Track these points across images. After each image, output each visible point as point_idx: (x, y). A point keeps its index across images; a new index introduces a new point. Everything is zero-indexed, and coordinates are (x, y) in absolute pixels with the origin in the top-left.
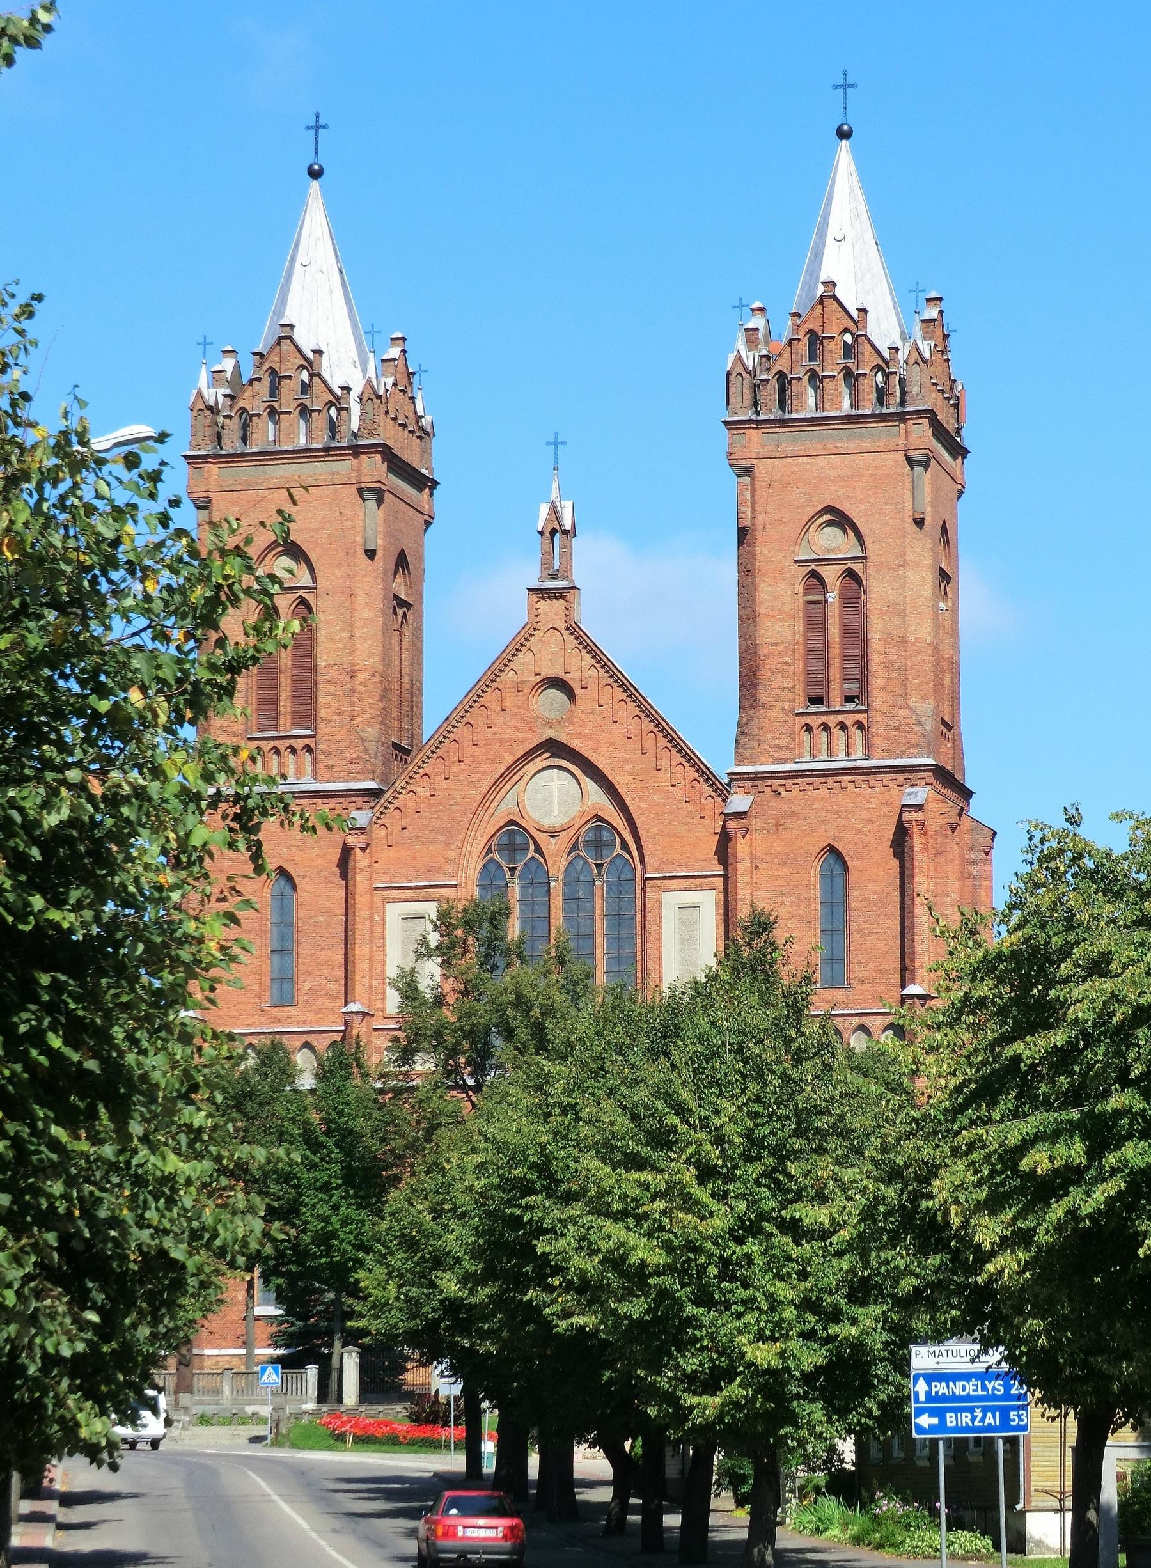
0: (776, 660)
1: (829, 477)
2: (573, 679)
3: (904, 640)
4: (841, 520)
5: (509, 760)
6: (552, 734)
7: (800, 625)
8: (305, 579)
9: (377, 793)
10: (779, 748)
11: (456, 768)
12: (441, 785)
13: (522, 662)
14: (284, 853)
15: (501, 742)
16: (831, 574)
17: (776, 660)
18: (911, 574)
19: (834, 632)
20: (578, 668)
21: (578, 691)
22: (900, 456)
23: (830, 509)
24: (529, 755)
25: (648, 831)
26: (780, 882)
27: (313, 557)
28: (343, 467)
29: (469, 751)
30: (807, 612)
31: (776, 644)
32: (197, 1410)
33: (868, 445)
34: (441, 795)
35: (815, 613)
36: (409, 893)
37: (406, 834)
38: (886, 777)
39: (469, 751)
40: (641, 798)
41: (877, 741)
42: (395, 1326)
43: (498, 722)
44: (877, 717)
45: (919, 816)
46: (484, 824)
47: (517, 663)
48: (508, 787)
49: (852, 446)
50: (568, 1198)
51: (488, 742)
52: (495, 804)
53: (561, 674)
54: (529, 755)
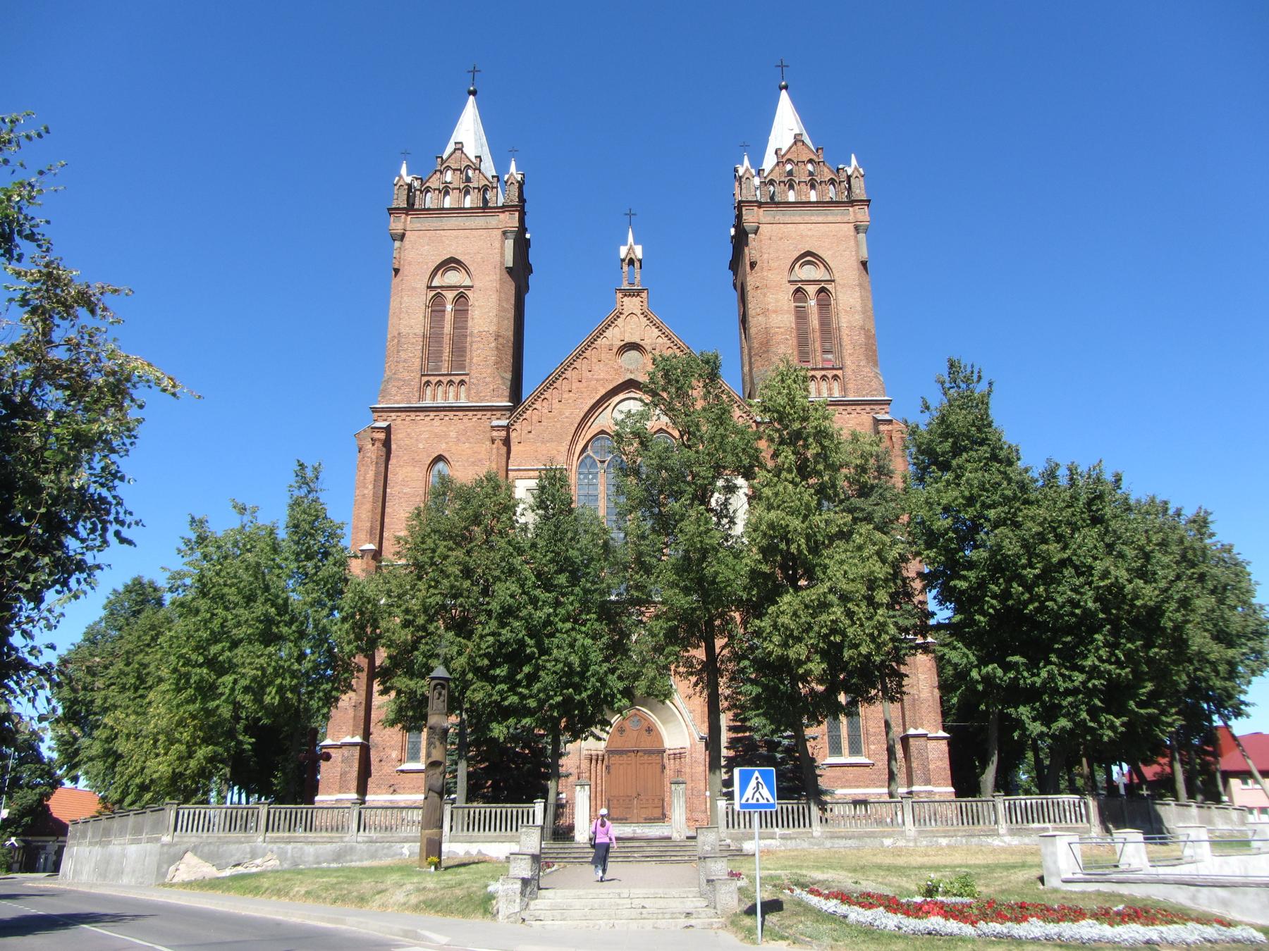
0: (780, 337)
5: (603, 392)
6: (632, 377)
7: (793, 319)
11: (566, 396)
12: (556, 405)
14: (444, 446)
16: (811, 290)
17: (780, 337)
22: (851, 226)
23: (809, 253)
27: (472, 268)
29: (575, 385)
30: (797, 312)
32: (244, 628)
33: (831, 219)
34: (555, 412)
35: (801, 315)
38: (858, 408)
41: (851, 386)
42: (770, 653)
43: (595, 368)
44: (848, 371)
45: (890, 427)
47: (608, 333)
49: (820, 219)
50: (308, 893)
51: (589, 380)
53: (638, 341)
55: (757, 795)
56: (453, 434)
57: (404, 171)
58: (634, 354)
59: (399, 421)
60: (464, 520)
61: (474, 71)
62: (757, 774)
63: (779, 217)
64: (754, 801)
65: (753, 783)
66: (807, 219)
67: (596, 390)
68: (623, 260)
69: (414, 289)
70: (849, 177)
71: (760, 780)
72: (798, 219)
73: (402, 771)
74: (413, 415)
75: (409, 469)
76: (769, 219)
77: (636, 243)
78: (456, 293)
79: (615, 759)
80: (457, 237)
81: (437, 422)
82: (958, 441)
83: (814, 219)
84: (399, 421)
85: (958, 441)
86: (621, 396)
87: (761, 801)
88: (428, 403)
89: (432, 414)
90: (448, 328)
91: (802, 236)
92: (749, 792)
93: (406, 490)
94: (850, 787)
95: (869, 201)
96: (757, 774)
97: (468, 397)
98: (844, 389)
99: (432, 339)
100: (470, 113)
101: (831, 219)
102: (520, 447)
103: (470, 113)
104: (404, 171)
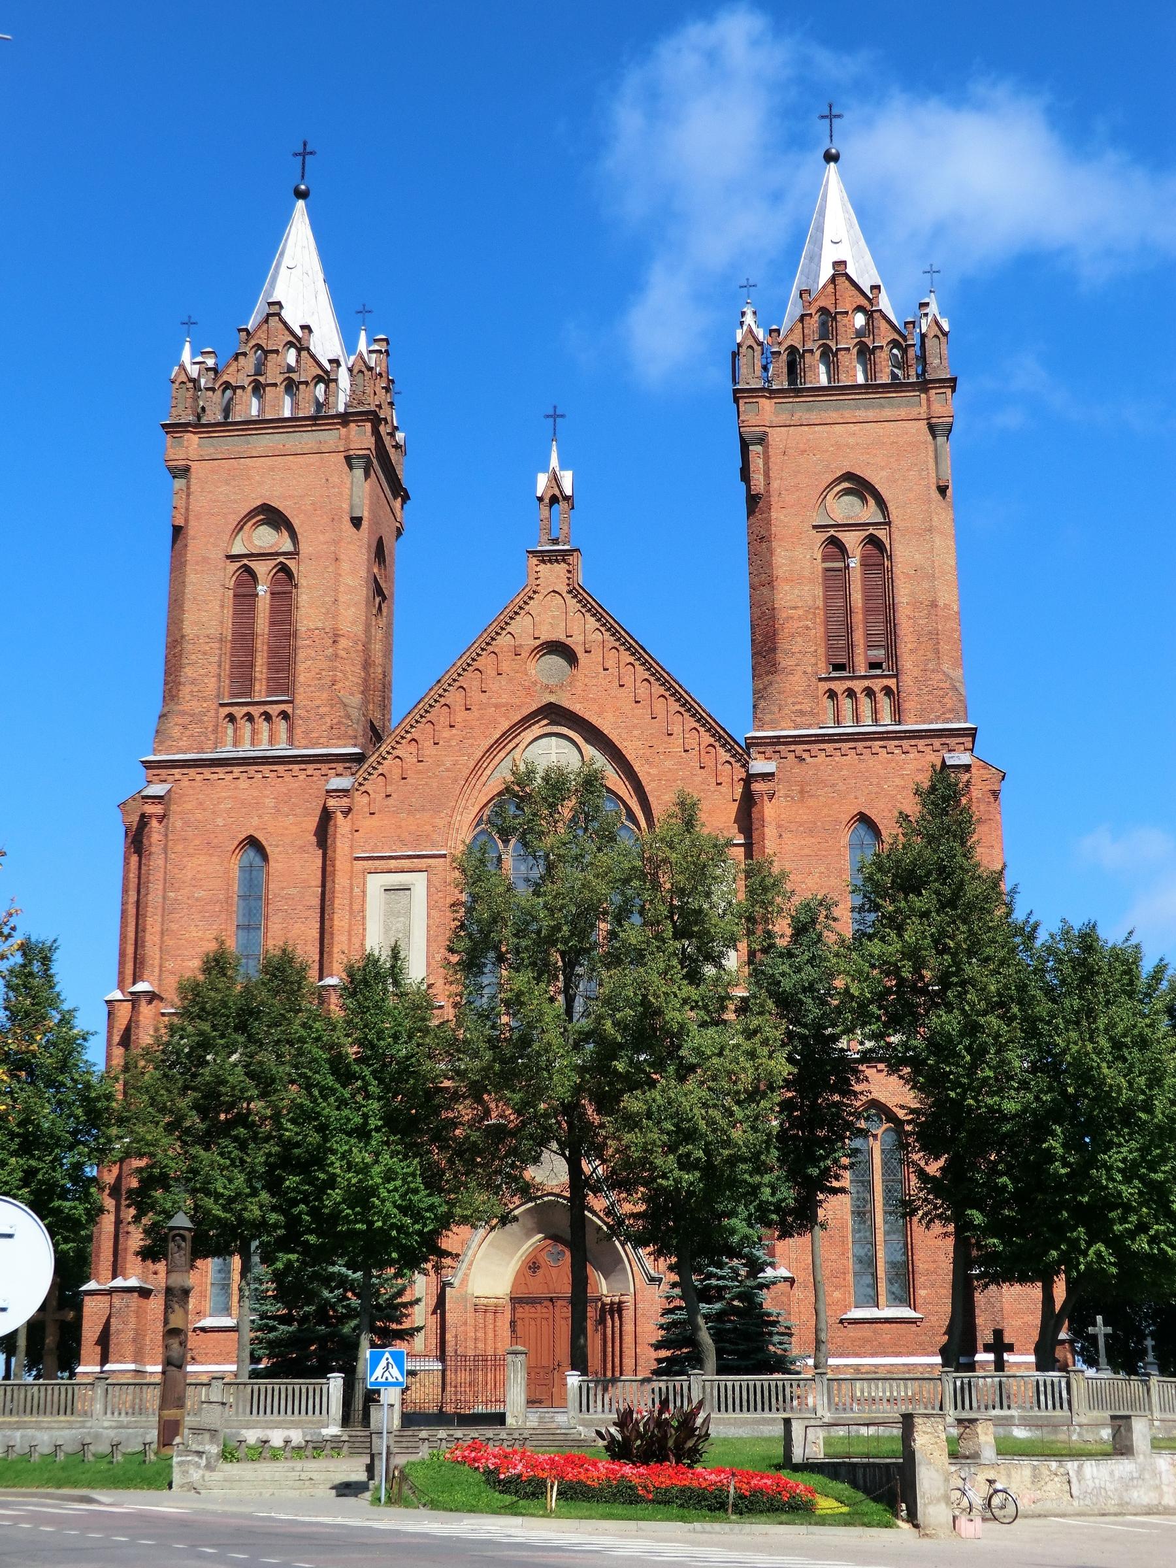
1: (847, 445)
2: (576, 643)
3: (934, 604)
4: (859, 486)
5: (506, 725)
7: (819, 591)
8: (288, 546)
9: (359, 759)
10: (802, 713)
11: (446, 733)
13: (521, 625)
14: (255, 821)
15: (496, 706)
18: (938, 541)
19: (262, 624)
20: (582, 631)
21: (580, 654)
22: (923, 425)
23: (849, 476)
24: (527, 721)
25: (658, 798)
26: (806, 851)
27: (296, 523)
28: (331, 438)
29: (460, 716)
31: (795, 608)
35: (835, 580)
36: (393, 864)
37: (390, 801)
39: (460, 716)
40: (651, 764)
43: (493, 685)
46: (475, 793)
47: (513, 627)
48: (502, 754)
52: (488, 772)
54: (527, 721)
55: (387, 1374)
56: (269, 802)
57: (186, 356)
58: (556, 661)
59: (185, 783)
60: (239, 1007)
61: (304, 154)
62: (387, 1355)
63: (801, 415)
64: (384, 1380)
65: (383, 1363)
66: (848, 415)
67: (494, 723)
68: (540, 499)
69: (205, 560)
70: (923, 336)
71: (391, 1360)
72: (833, 416)
73: (203, 1330)
74: (207, 772)
75: (203, 859)
76: (784, 418)
77: (562, 468)
78: (273, 563)
79: (524, 1312)
80: (272, 469)
81: (243, 784)
82: (930, 872)
83: (861, 414)
84: (185, 783)
85: (930, 872)
86: (536, 730)
87: (390, 1379)
88: (227, 751)
89: (237, 770)
90: (262, 624)
91: (838, 446)
92: (379, 1372)
93: (200, 894)
94: (886, 1355)
95: (954, 380)
96: (387, 1355)
97: (291, 741)
98: (898, 714)
99: (243, 638)
100: (300, 240)
101: (888, 413)
102: (373, 822)
103: (300, 240)
104: (186, 356)
